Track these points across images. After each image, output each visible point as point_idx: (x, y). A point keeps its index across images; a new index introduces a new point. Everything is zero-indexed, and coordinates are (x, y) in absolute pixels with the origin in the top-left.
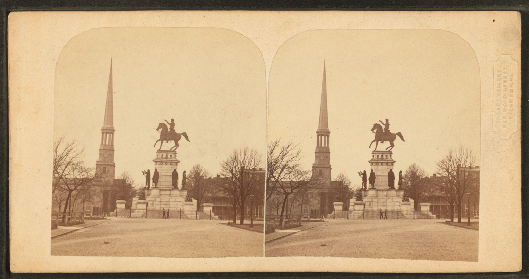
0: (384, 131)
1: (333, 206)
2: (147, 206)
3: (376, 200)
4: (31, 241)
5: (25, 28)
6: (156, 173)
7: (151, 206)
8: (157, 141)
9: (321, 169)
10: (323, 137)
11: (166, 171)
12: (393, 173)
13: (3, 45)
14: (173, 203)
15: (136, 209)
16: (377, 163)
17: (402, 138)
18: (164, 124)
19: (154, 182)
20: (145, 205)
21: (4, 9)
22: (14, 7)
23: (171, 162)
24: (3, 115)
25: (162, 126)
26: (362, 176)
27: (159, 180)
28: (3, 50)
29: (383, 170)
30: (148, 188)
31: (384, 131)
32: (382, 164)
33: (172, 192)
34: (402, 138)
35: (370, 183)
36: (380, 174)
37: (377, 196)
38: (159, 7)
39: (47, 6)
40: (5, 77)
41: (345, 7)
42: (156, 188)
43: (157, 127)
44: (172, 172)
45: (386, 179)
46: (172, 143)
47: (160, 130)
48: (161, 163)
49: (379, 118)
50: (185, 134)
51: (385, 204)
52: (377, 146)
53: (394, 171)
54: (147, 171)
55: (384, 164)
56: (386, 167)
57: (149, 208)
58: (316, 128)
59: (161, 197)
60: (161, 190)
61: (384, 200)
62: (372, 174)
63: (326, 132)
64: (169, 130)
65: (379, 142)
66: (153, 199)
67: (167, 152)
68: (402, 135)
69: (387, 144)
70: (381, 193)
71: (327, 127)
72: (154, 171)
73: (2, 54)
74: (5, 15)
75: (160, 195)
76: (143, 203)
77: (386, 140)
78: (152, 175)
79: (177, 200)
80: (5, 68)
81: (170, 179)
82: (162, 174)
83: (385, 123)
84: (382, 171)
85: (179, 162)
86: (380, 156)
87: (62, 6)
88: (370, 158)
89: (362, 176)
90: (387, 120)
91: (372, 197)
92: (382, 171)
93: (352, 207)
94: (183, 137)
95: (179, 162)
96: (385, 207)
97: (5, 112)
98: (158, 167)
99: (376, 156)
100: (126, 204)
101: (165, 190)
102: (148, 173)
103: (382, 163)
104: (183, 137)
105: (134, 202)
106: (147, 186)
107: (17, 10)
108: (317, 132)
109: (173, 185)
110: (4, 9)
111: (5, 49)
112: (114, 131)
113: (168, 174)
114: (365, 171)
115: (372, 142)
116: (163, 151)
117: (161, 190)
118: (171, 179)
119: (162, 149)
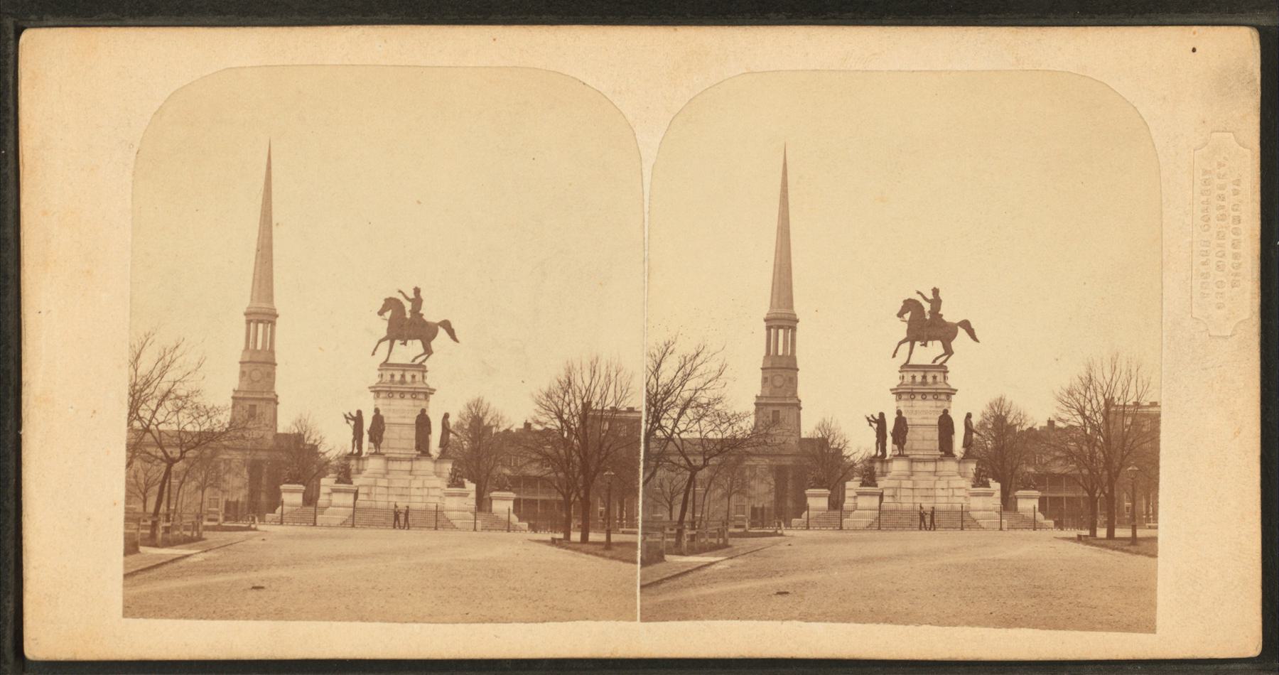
0: (928, 317)
1: (805, 498)
2: (356, 498)
3: (909, 484)
4: (75, 583)
5: (61, 67)
6: (378, 420)
7: (364, 497)
8: (380, 342)
9: (776, 408)
10: (781, 332)
11: (400, 413)
12: (950, 419)
13: (7, 110)
14: (419, 492)
15: (330, 505)
16: (912, 393)
17: (971, 333)
18: (397, 301)
19: (371, 440)
20: (351, 497)
21: (9, 23)
22: (33, 17)
23: (414, 393)
24: (6, 277)
25: (391, 304)
26: (875, 425)
27: (385, 435)
28: (7, 121)
29: (926, 412)
30: (358, 456)
31: (928, 317)
32: (924, 396)
33: (417, 465)
34: (971, 333)
35: (894, 442)
36: (920, 422)
37: (912, 473)
38: (385, 16)
39: (114, 15)
40: (12, 187)
41: (834, 18)
42: (377, 454)
43: (380, 307)
44: (937, 417)
45: (934, 434)
46: (416, 347)
47: (388, 314)
48: (390, 394)
49: (917, 286)
50: (446, 325)
51: (930, 493)
52: (911, 353)
53: (952, 414)
54: (355, 414)
55: (930, 397)
56: (933, 403)
57: (360, 503)
58: (764, 310)
59: (389, 477)
60: (388, 459)
61: (930, 484)
62: (900, 421)
63: (789, 320)
64: (408, 316)
65: (917, 344)
66: (894, 483)
67: (404, 367)
68: (973, 326)
69: (936, 348)
70: (920, 467)
71: (791, 307)
72: (373, 414)
73: (6, 132)
74: (12, 36)
75: (388, 472)
76: (346, 491)
77: (933, 338)
78: (890, 426)
79: (954, 484)
80: (11, 165)
81: (412, 434)
82: (392, 420)
83: (930, 296)
84: (923, 414)
85: (432, 391)
86: (919, 379)
87: (149, 14)
88: (895, 382)
89: (875, 425)
90: (936, 291)
91: (899, 478)
92: (923, 414)
93: (851, 501)
94: (442, 332)
95: (432, 391)
96: (931, 501)
97: (11, 271)
98: (382, 404)
99: (908, 378)
100: (304, 493)
101: (400, 460)
102: (358, 419)
103: (924, 394)
104: (442, 332)
105: (323, 490)
106: (356, 451)
107: (40, 24)
108: (766, 320)
109: (418, 448)
110: (9, 23)
111: (11, 118)
112: (277, 316)
113: (407, 421)
114: (882, 415)
115: (900, 343)
116: (393, 365)
117: (388, 459)
118: (414, 433)
119: (391, 361)
